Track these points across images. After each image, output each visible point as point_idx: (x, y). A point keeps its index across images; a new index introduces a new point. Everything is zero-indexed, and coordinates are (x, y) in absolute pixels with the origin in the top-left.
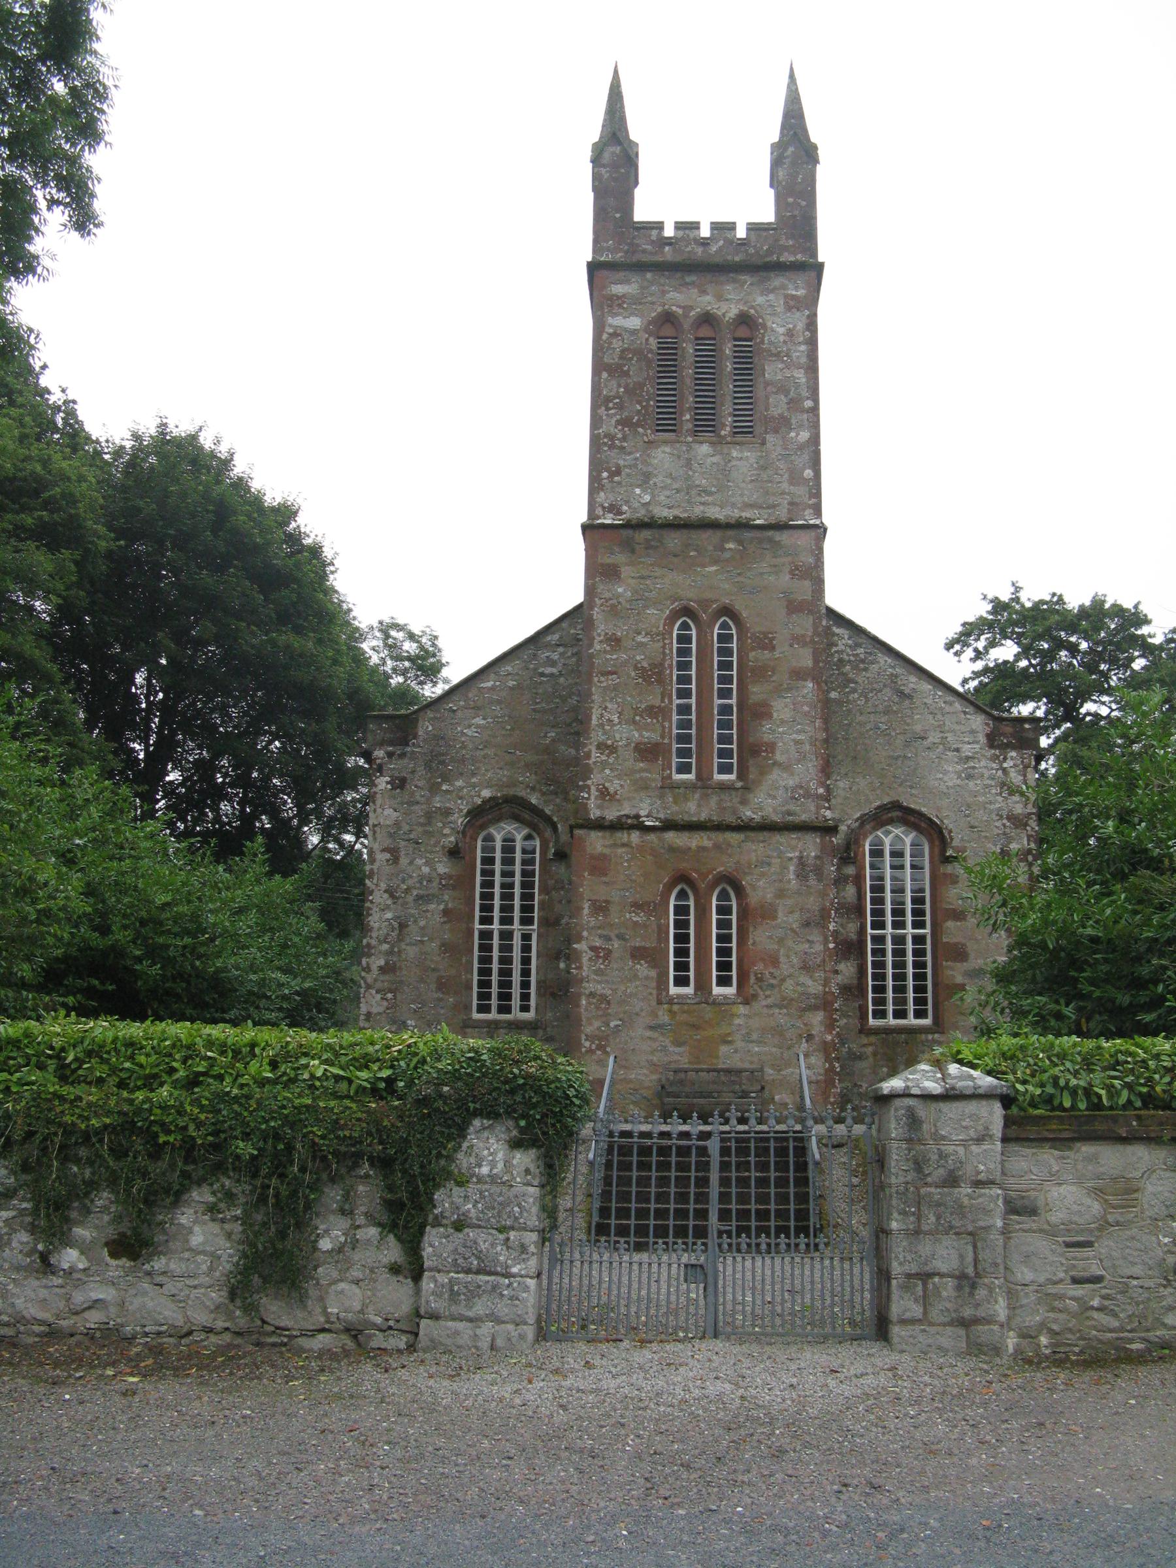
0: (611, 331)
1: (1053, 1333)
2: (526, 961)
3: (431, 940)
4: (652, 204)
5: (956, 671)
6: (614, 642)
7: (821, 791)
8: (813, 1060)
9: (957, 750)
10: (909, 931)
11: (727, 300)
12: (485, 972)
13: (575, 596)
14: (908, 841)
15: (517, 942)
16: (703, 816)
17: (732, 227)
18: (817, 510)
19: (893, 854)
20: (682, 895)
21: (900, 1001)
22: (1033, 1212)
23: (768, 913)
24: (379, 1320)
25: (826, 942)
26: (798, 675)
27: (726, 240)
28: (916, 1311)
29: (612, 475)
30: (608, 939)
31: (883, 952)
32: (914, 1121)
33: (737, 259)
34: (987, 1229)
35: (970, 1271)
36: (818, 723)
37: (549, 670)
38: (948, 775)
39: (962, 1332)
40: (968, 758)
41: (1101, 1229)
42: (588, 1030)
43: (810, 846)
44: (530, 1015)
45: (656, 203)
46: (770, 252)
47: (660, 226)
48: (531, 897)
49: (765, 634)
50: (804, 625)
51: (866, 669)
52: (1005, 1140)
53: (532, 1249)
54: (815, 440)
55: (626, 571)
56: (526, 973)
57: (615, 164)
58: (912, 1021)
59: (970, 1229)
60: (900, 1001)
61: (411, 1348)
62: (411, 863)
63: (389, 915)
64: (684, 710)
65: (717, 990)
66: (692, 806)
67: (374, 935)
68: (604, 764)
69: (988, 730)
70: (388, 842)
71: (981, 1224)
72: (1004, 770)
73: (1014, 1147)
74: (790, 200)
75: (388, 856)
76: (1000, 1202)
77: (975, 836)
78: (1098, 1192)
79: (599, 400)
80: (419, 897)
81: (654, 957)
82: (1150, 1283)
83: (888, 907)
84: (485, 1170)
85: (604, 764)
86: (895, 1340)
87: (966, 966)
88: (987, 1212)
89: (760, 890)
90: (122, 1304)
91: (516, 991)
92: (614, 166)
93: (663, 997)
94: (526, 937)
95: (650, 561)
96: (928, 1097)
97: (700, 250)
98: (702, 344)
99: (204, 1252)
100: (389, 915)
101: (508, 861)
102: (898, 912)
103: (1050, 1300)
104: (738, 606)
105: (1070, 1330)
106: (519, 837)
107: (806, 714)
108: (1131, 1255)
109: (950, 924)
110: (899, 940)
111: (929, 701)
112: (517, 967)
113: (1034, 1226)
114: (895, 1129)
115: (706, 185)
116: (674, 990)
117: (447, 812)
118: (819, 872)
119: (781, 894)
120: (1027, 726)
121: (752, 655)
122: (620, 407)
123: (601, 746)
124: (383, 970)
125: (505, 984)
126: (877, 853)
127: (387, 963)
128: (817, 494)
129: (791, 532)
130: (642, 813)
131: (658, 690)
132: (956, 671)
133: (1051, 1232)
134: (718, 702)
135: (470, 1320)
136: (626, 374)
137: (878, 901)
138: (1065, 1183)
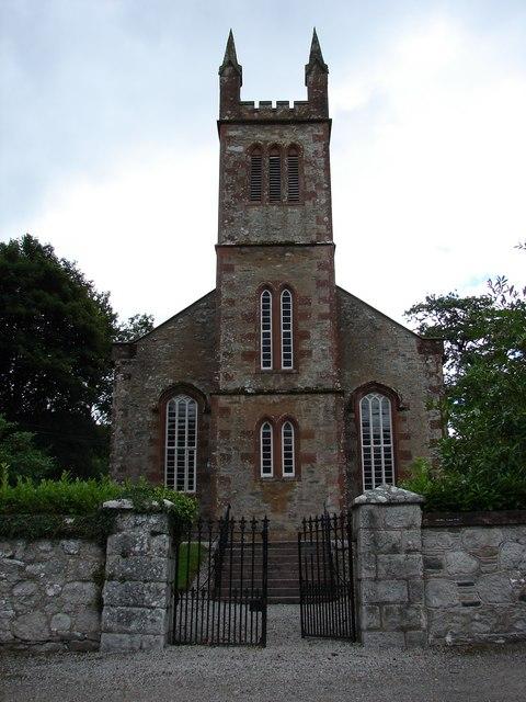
1: (454, 635)
2: (191, 464)
4: (250, 93)
6: (232, 302)
10: (382, 445)
11: (287, 137)
13: (211, 285)
15: (187, 455)
17: (287, 103)
18: (331, 236)
20: (267, 427)
22: (439, 566)
23: (310, 435)
24: (79, 634)
26: (323, 317)
27: (285, 110)
28: (376, 623)
32: (372, 517)
34: (414, 577)
42: (221, 495)
43: (331, 399)
46: (305, 115)
47: (252, 103)
54: (329, 202)
55: (237, 268)
56: (191, 470)
57: (231, 75)
59: (405, 576)
62: (134, 416)
63: (122, 443)
65: (285, 475)
73: (428, 531)
76: (421, 562)
78: (474, 555)
79: (223, 186)
84: (137, 549)
85: (226, 363)
88: (413, 567)
89: (304, 424)
91: (186, 479)
92: (230, 76)
94: (191, 452)
96: (380, 504)
97: (272, 115)
98: (274, 160)
100: (122, 443)
104: (292, 284)
108: (496, 590)
110: (377, 450)
113: (440, 575)
115: (274, 82)
116: (263, 475)
117: (153, 391)
122: (233, 189)
123: (225, 354)
124: (119, 469)
125: (181, 476)
128: (330, 228)
129: (321, 246)
132: (413, 325)
135: (129, 633)
138: (457, 550)
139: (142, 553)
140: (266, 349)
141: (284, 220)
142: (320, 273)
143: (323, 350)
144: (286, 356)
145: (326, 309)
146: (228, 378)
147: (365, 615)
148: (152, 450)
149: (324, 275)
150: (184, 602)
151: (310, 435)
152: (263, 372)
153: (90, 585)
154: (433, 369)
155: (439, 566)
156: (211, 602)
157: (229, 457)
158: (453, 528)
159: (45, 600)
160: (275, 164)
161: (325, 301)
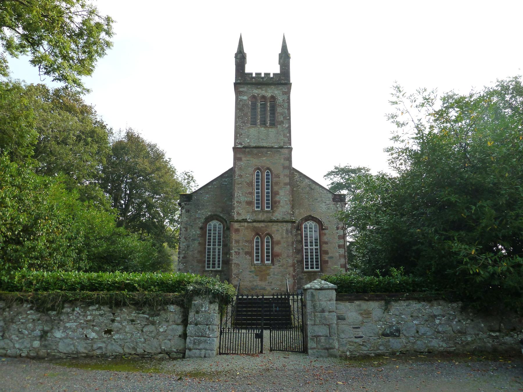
1: (350, 352)
2: (219, 255)
5: (326, 183)
6: (241, 176)
8: (290, 279)
11: (268, 92)
12: (209, 258)
13: (231, 165)
14: (313, 225)
15: (217, 250)
16: (263, 219)
17: (269, 74)
18: (290, 144)
21: (312, 265)
22: (344, 319)
23: (278, 243)
24: (175, 350)
25: (293, 250)
26: (286, 184)
28: (314, 345)
30: (239, 249)
31: (307, 252)
32: (313, 295)
38: (323, 207)
39: (326, 351)
41: (362, 324)
43: (289, 226)
44: (220, 269)
45: (252, 68)
50: (287, 172)
52: (336, 300)
54: (289, 127)
55: (243, 159)
56: (219, 258)
57: (241, 58)
58: (315, 270)
60: (312, 265)
61: (184, 357)
63: (185, 244)
64: (258, 193)
65: (266, 262)
66: (260, 217)
70: (185, 226)
73: (339, 302)
78: (361, 314)
80: (192, 239)
81: (250, 254)
82: (375, 338)
84: (203, 309)
85: (238, 206)
86: (309, 353)
89: (277, 237)
90: (106, 348)
91: (216, 263)
93: (252, 264)
96: (316, 289)
98: (263, 101)
100: (185, 244)
101: (215, 230)
102: (311, 242)
105: (355, 351)
106: (217, 225)
109: (324, 245)
110: (311, 249)
114: (308, 297)
116: (255, 262)
117: (199, 218)
118: (291, 232)
119: (282, 238)
122: (242, 118)
126: (306, 228)
132: (326, 183)
135: (199, 349)
137: (306, 240)
138: (351, 310)
139: (205, 311)
140: (257, 200)
143: (285, 201)
144: (267, 204)
145: (287, 180)
147: (309, 342)
149: (287, 163)
151: (278, 243)
152: (255, 211)
153: (180, 326)
154: (340, 209)
155: (344, 319)
157: (239, 253)
158: (351, 301)
159: (158, 333)
160: (264, 106)
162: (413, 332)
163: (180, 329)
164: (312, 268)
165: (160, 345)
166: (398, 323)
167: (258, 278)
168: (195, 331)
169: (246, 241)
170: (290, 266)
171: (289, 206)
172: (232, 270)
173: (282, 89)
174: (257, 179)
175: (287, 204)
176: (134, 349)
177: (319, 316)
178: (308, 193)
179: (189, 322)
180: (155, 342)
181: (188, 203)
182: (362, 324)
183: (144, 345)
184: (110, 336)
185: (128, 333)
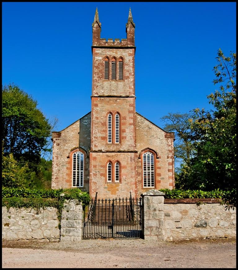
0: (96, 60)
2: (82, 177)
3: (64, 173)
6: (97, 118)
7: (135, 145)
9: (159, 138)
15: (80, 173)
19: (148, 157)
22: (169, 216)
23: (125, 167)
24: (53, 237)
26: (130, 124)
28: (149, 233)
29: (96, 87)
33: (120, 46)
35: (158, 226)
36: (134, 133)
37: (85, 124)
39: (156, 237)
40: (161, 140)
41: (181, 219)
43: (133, 154)
44: (83, 186)
46: (126, 45)
48: (83, 165)
49: (125, 117)
51: (143, 124)
53: (80, 223)
55: (99, 105)
56: (82, 179)
62: (61, 159)
63: (56, 169)
64: (110, 131)
65: (116, 181)
66: (111, 148)
67: (54, 172)
68: (95, 140)
69: (165, 135)
70: (56, 155)
71: (160, 218)
72: (168, 142)
74: (130, 35)
75: (56, 158)
77: (162, 154)
78: (181, 212)
83: (147, 167)
84: (72, 209)
85: (95, 140)
87: (161, 177)
89: (123, 163)
91: (80, 182)
93: (106, 182)
94: (82, 172)
95: (104, 103)
97: (113, 44)
99: (21, 225)
102: (149, 168)
103: (172, 231)
106: (80, 154)
107: (132, 131)
111: (154, 129)
112: (80, 178)
116: (108, 181)
117: (67, 150)
118: (134, 160)
119: (128, 164)
120: (172, 134)
121: (122, 121)
122: (98, 74)
123: (95, 137)
126: (145, 157)
127: (56, 177)
130: (102, 149)
131: (105, 127)
133: (172, 220)
134: (108, 129)
136: (99, 68)
138: (175, 210)
139: (73, 210)
140: (109, 136)
141: (117, 87)
142: (130, 108)
143: (130, 137)
144: (117, 139)
145: (132, 121)
146: (95, 146)
148: (67, 172)
150: (87, 226)
152: (109, 144)
155: (169, 216)
156: (131, 226)
157: (96, 175)
161: (132, 119)
162: (215, 224)
163: (57, 223)
164: (149, 186)
165: (43, 233)
166: (206, 219)
167: (110, 193)
168: (67, 224)
169: (101, 166)
170: (133, 184)
171: (133, 141)
172: (91, 187)
173: (128, 51)
174: (109, 120)
175: (131, 139)
176: (25, 235)
177: (152, 213)
178: (147, 131)
179: (62, 218)
180: (40, 232)
181: (58, 138)
182: (181, 219)
183: (32, 233)
184: (8, 227)
185: (20, 225)
